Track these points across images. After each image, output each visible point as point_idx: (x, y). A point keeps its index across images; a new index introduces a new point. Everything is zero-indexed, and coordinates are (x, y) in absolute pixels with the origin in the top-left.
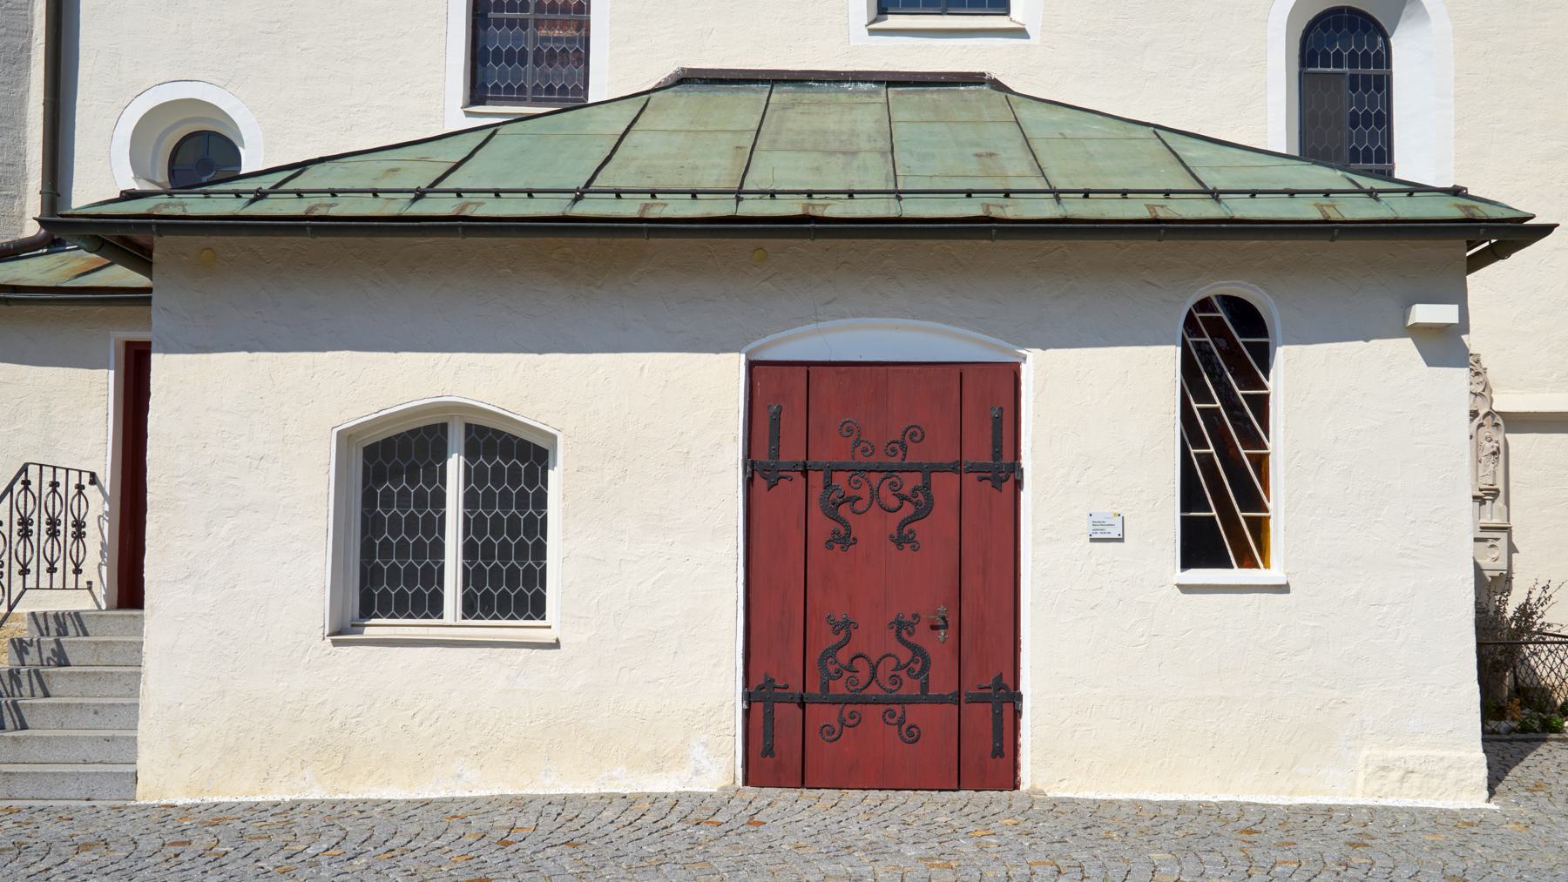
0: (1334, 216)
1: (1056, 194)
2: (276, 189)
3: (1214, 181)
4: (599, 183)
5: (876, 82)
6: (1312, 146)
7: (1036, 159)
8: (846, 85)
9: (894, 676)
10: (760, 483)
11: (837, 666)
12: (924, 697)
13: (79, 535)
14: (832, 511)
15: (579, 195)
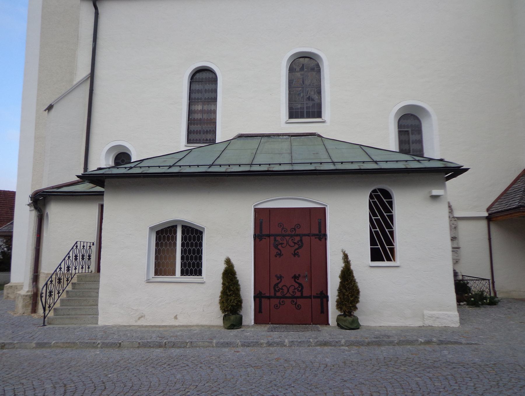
0: (409, 167)
1: (334, 163)
2: (135, 167)
3: (376, 158)
4: (216, 163)
5: (288, 136)
6: (403, 151)
7: (329, 154)
8: (281, 137)
9: (293, 291)
10: (258, 240)
11: (278, 288)
12: (302, 297)
13: (89, 259)
14: (276, 247)
15: (210, 166)
